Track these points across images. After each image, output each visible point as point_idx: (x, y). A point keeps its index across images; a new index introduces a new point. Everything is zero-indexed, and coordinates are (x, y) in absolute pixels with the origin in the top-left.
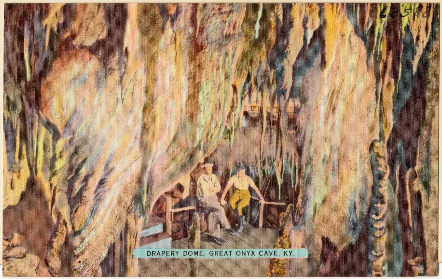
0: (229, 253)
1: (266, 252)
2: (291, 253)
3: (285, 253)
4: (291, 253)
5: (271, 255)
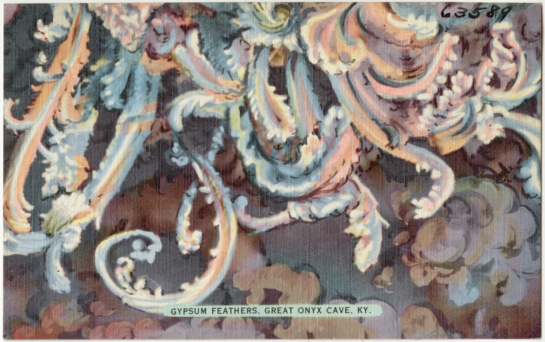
0: (289, 310)
1: (335, 308)
2: (366, 310)
3: (359, 310)
4: (366, 310)
5: (341, 312)
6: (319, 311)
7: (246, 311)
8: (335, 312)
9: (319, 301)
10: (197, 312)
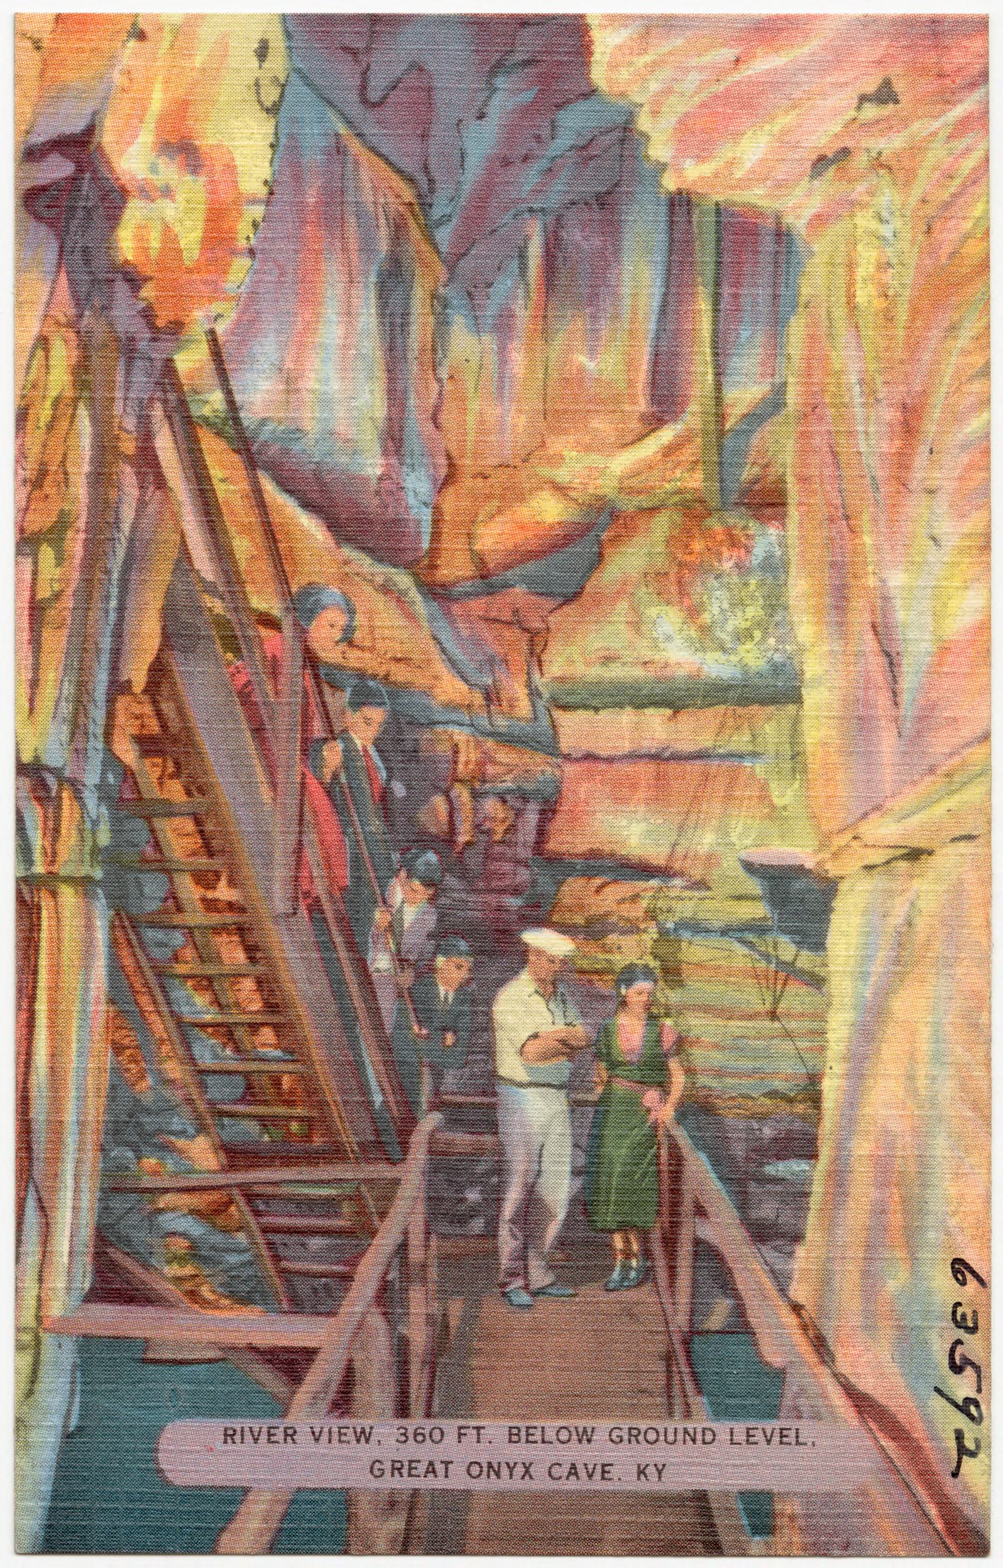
0: (440, 1468)
2: (660, 1472)
4: (660, 1472)
6: (527, 1471)
7: (280, 1436)
8: (431, 1476)
9: (271, 1549)
10: (671, 1438)
